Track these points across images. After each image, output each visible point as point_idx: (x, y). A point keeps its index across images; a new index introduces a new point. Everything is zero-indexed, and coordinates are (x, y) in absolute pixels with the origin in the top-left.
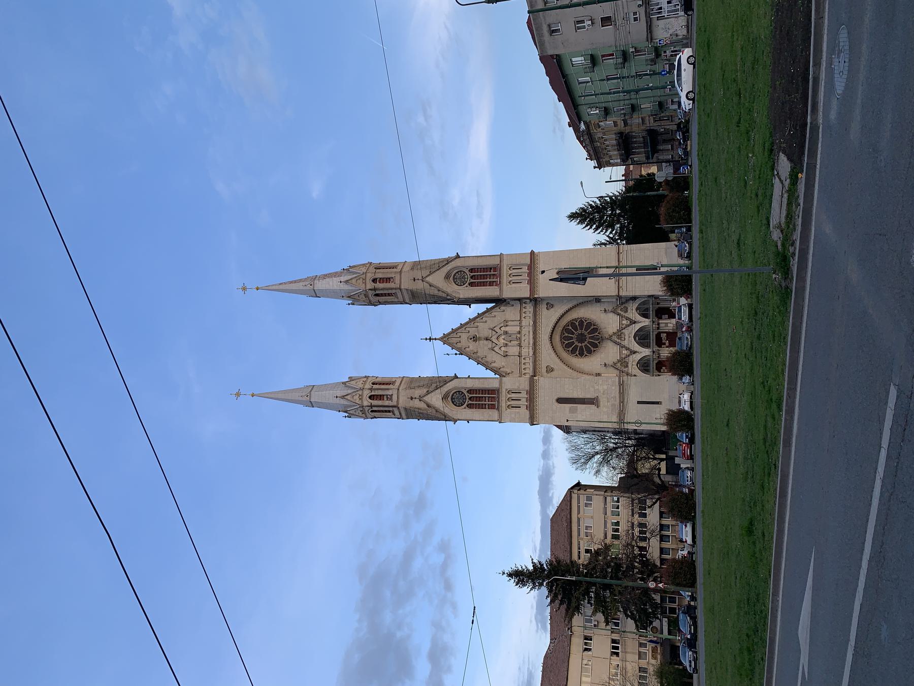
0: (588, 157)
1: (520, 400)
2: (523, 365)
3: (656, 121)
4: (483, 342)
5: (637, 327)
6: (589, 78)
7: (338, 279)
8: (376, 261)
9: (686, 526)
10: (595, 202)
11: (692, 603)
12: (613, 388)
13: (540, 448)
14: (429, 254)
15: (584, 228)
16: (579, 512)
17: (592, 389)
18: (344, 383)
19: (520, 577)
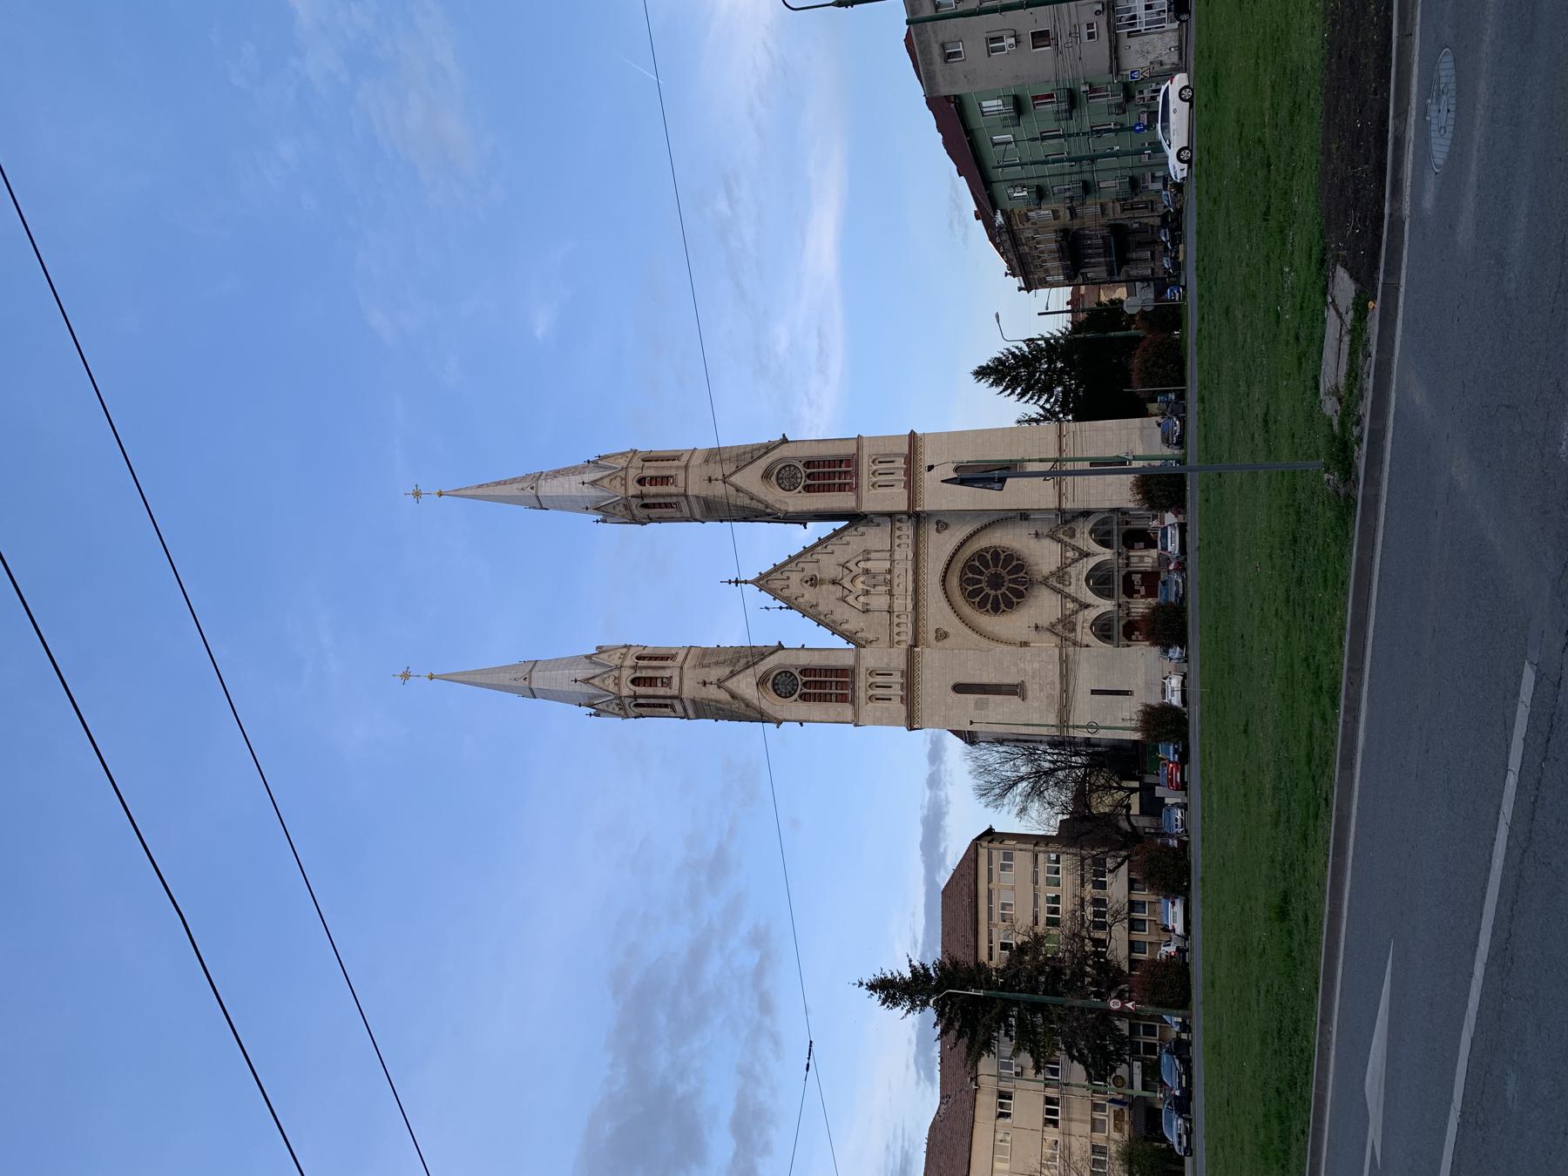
0: (1009, 272)
2: (895, 618)
3: (1125, 210)
7: (579, 478)
8: (644, 447)
9: (1173, 904)
10: (1020, 349)
12: (1050, 667)
13: (925, 769)
15: (1001, 392)
16: (990, 880)
17: (1014, 669)
18: (589, 657)
19: (890, 990)
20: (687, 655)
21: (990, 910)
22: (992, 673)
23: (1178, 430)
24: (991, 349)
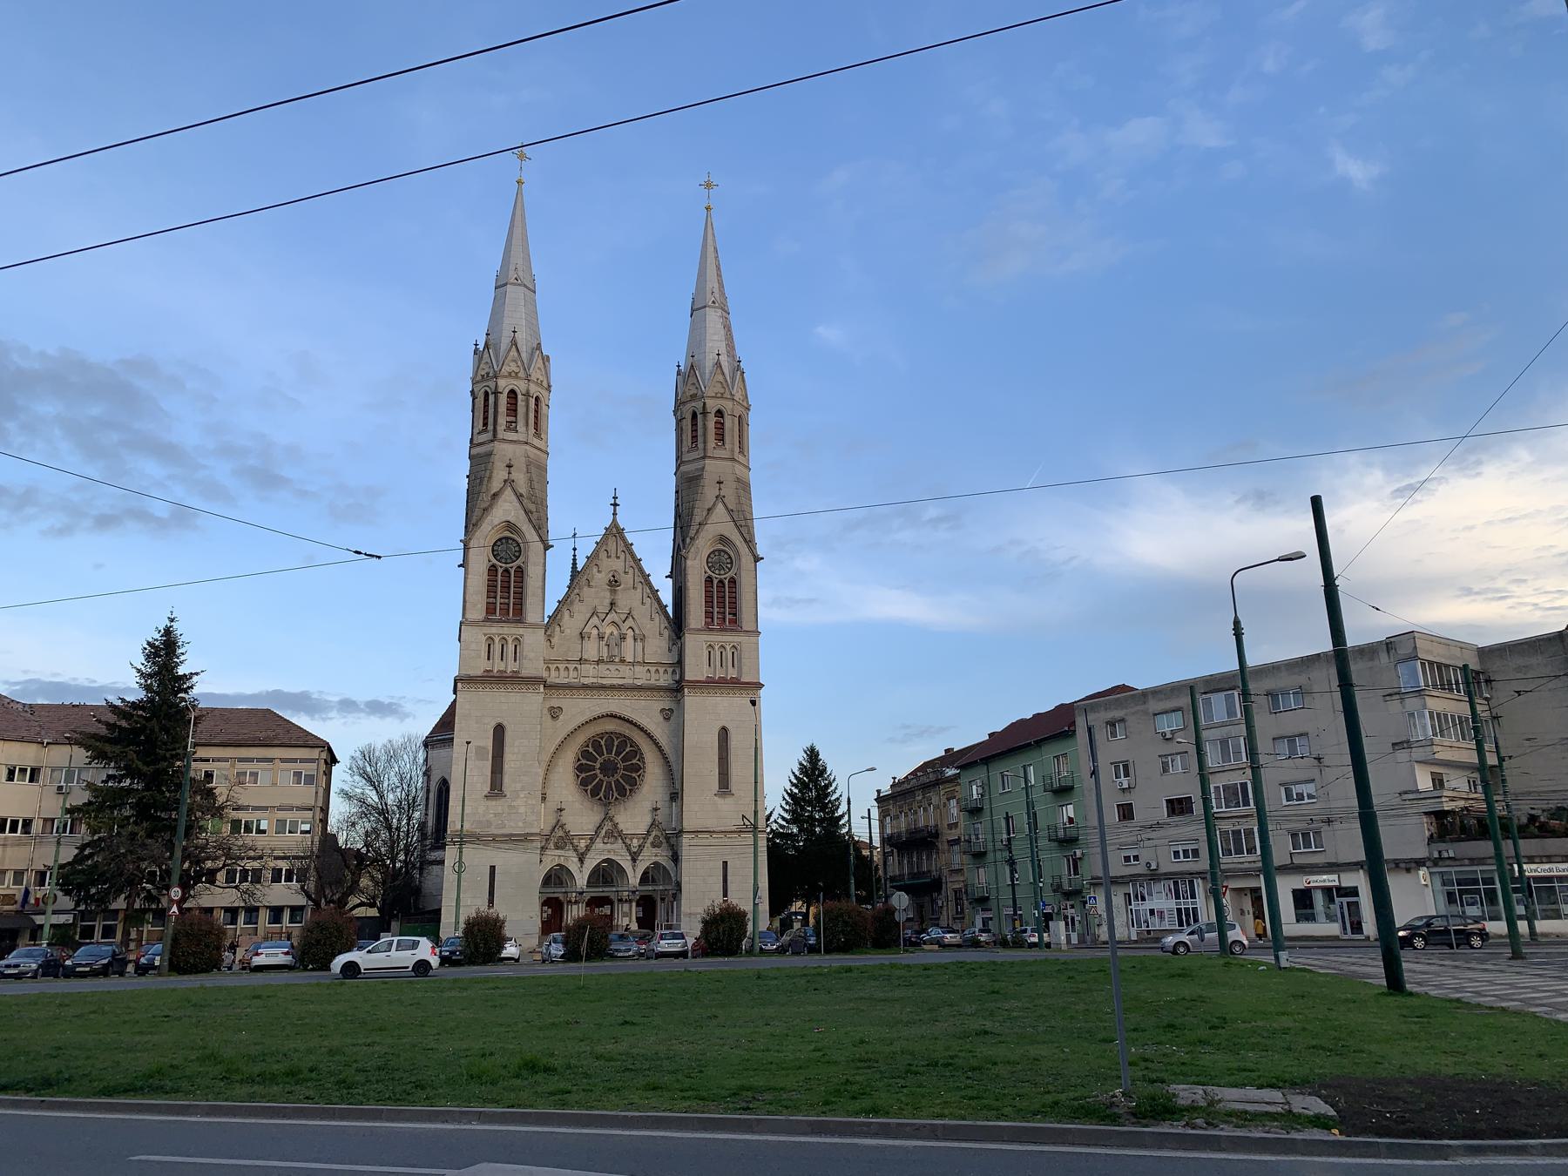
0: (897, 781)
1: (502, 659)
2: (655, 668)
3: (956, 892)
4: (607, 597)
5: (626, 864)
6: (1033, 783)
7: (723, 350)
8: (753, 419)
9: (287, 953)
10: (834, 792)
11: (130, 968)
12: (521, 824)
13: (361, 697)
14: (760, 508)
15: (793, 773)
16: (283, 760)
17: (519, 786)
18: (539, 347)
19: (164, 651)
20: (539, 449)
21: (251, 760)
22: (515, 764)
23: (767, 948)
24: (837, 767)
